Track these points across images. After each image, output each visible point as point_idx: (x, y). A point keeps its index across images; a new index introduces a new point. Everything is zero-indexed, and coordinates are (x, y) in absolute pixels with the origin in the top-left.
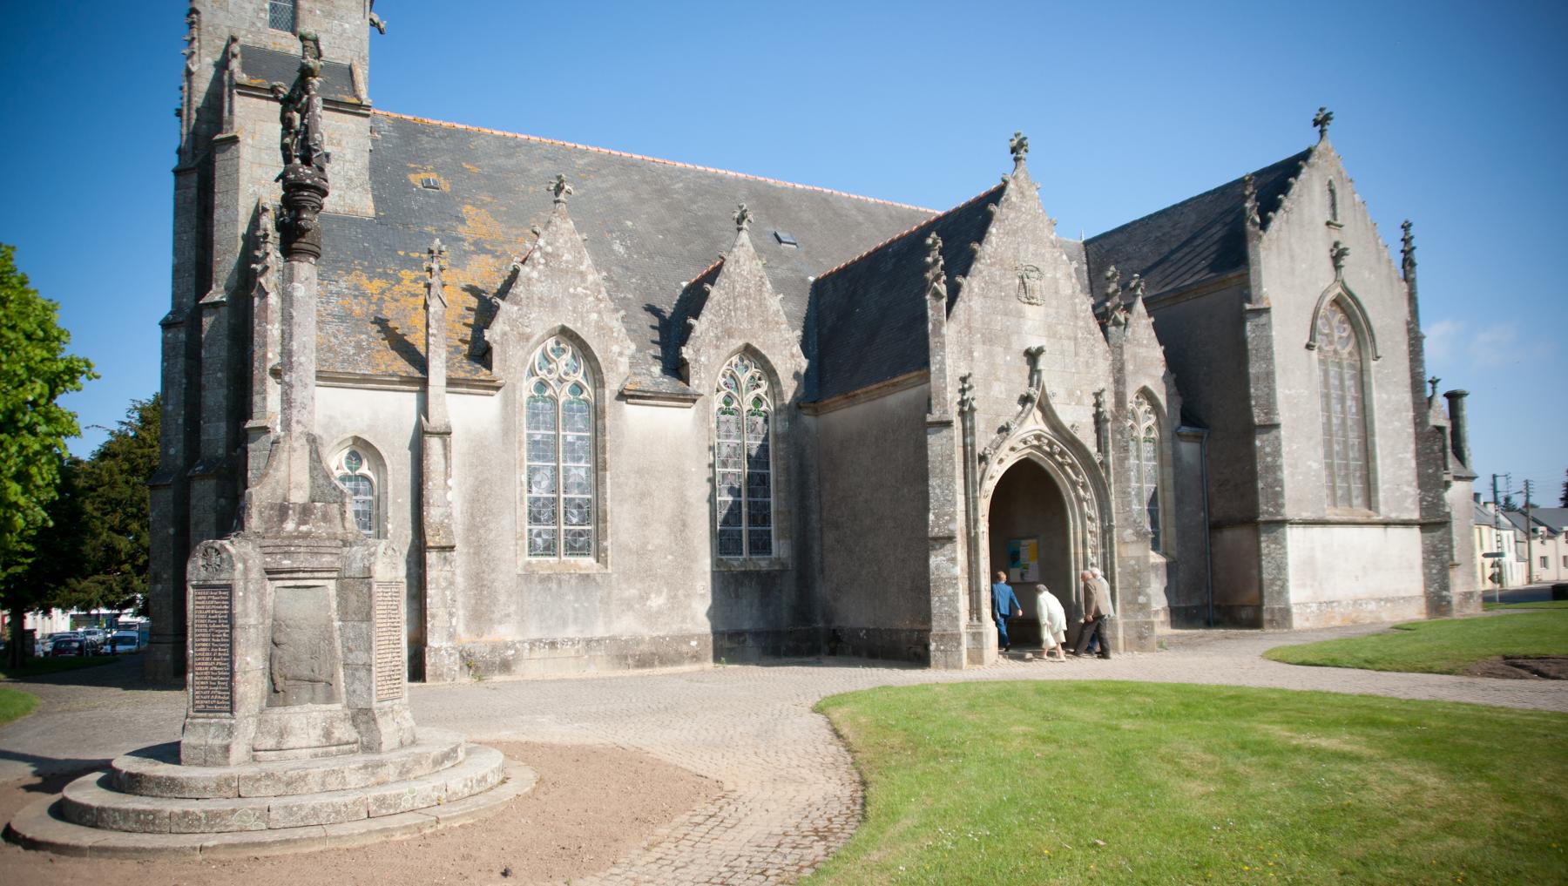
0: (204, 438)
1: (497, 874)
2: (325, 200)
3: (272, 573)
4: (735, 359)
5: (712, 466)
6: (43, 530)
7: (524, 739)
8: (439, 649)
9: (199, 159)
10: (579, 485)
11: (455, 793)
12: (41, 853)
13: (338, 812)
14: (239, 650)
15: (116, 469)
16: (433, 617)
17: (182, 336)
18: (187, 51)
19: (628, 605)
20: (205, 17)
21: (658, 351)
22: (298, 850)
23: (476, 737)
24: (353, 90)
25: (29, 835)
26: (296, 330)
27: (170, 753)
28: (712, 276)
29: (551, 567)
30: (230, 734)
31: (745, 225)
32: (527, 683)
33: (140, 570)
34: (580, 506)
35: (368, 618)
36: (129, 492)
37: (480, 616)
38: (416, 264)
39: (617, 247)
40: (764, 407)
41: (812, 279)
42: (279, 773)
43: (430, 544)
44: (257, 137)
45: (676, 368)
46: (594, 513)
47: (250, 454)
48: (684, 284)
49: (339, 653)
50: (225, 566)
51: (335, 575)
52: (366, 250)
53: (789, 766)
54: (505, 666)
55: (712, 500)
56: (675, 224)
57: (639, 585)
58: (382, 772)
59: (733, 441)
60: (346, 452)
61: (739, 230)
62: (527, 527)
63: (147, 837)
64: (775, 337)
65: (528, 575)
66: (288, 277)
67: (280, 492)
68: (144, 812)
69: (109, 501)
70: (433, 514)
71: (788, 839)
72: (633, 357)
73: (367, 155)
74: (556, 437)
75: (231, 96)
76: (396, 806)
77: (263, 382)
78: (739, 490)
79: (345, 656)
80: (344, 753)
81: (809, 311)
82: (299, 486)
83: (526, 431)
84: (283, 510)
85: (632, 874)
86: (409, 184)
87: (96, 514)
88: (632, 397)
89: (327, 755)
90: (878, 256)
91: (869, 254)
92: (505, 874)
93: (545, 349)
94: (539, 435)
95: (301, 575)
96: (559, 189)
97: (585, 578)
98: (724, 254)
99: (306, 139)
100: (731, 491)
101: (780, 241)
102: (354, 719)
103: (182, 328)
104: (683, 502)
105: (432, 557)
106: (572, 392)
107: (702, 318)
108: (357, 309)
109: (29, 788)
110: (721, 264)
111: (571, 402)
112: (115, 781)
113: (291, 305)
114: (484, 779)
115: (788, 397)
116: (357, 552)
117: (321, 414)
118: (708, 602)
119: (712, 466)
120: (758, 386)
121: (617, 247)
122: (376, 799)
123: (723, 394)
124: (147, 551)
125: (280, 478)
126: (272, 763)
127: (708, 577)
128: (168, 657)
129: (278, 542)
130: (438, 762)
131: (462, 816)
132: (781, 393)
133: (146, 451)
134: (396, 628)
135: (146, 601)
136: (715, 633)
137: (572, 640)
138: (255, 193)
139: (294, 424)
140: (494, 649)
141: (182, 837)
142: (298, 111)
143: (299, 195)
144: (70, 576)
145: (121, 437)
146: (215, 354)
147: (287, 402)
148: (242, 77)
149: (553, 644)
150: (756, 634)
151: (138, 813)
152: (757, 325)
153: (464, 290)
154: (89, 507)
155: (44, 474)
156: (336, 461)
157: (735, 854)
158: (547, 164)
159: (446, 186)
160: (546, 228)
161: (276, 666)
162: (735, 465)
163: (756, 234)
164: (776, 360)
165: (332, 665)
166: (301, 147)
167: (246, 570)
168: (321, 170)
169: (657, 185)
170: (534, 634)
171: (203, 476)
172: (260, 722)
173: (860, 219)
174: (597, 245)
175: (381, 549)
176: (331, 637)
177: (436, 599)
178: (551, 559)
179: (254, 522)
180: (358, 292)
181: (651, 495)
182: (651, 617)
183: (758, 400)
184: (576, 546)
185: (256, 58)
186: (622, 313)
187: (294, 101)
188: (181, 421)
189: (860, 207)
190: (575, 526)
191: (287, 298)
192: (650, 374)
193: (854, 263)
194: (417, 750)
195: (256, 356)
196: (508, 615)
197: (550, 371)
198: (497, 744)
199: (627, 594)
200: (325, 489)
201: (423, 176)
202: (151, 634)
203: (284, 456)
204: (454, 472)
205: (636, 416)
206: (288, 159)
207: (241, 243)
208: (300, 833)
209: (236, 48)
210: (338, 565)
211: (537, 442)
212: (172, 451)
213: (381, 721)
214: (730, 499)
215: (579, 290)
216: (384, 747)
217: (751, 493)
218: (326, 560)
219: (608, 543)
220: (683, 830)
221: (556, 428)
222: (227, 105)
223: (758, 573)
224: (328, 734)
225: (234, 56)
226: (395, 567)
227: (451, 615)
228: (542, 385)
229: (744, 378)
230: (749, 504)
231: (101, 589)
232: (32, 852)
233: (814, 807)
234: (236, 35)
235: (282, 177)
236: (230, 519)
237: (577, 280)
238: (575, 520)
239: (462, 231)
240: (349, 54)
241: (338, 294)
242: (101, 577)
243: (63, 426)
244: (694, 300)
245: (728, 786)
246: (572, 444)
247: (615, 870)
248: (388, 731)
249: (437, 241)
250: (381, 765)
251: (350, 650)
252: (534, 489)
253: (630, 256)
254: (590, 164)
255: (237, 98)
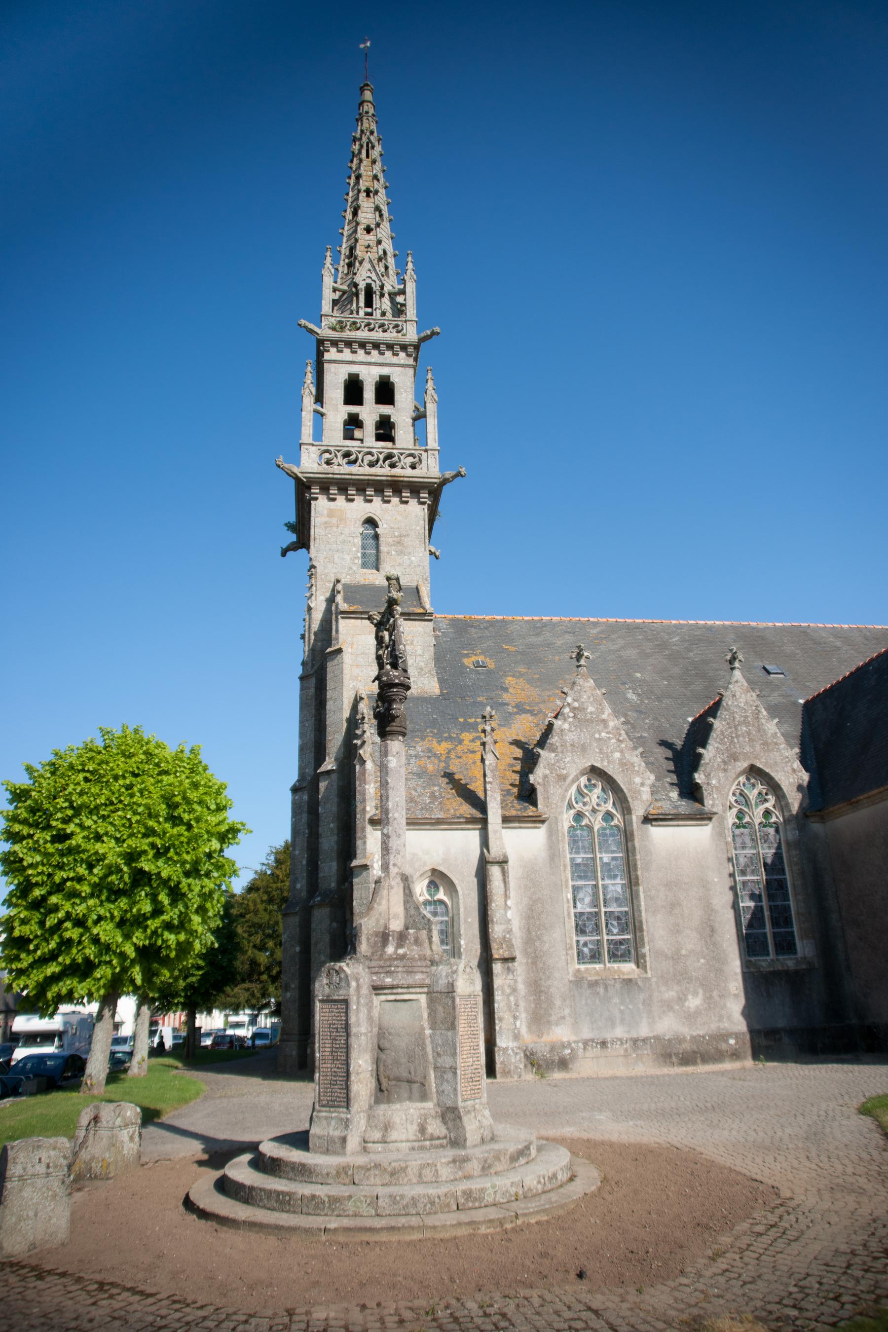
0: (321, 875)
1: (572, 1276)
2: (408, 693)
3: (377, 989)
4: (742, 779)
5: (732, 875)
6: (211, 950)
7: (585, 1136)
8: (506, 1049)
9: (316, 668)
10: (617, 899)
11: (530, 1189)
12: (209, 1223)
13: (433, 1203)
14: (354, 1054)
15: (258, 901)
16: (501, 1020)
17: (305, 797)
18: (308, 595)
19: (668, 1006)
20: (319, 570)
21: (673, 778)
22: (401, 1238)
23: (543, 1133)
24: (420, 604)
25: (201, 1206)
26: (391, 793)
27: (300, 1140)
28: (713, 710)
29: (597, 973)
30: (347, 1126)
31: (737, 664)
32: (584, 1080)
33: (274, 979)
34: (618, 918)
35: (453, 1026)
36: (267, 917)
37: (540, 1018)
38: (473, 727)
39: (631, 695)
40: (774, 819)
41: (802, 701)
42: (385, 1164)
43: (496, 956)
44: (355, 646)
45: (691, 792)
46: (631, 923)
47: (355, 887)
48: (690, 719)
49: (430, 1057)
50: (343, 984)
51: (426, 990)
52: (435, 720)
53: (844, 1173)
54: (563, 1064)
55: (735, 906)
56: (676, 671)
57: (676, 988)
58: (468, 1167)
59: (749, 852)
60: (426, 882)
61: (733, 669)
62: (575, 938)
63: (284, 1215)
64: (775, 756)
65: (579, 981)
66: (385, 753)
67: (382, 922)
68: (283, 1193)
69: (254, 925)
70: (496, 931)
71: (857, 1260)
72: (653, 786)
73: (432, 649)
74: (594, 859)
75: (337, 621)
76: (481, 1199)
77: (363, 829)
78: (760, 896)
79: (435, 1060)
80: (436, 1147)
81: (803, 729)
82: (396, 916)
83: (568, 856)
84: (384, 937)
85: (701, 1286)
86: (463, 666)
87: (246, 935)
88: (656, 820)
89: (422, 1148)
90: (859, 674)
91: (852, 674)
92: (581, 1275)
93: (579, 787)
94: (579, 858)
95: (400, 990)
96: (579, 656)
97: (628, 982)
98: (722, 691)
99: (394, 650)
100: (752, 896)
101: (769, 673)
102: (443, 1117)
103: (305, 789)
104: (709, 910)
105: (497, 967)
106: (604, 819)
107: (710, 747)
108: (430, 767)
109: (201, 1163)
110: (720, 701)
111: (604, 829)
112: (264, 1164)
113: (387, 774)
114: (555, 1176)
115: (795, 807)
116: (443, 970)
117: (409, 853)
118: (742, 1001)
119: (732, 875)
120: (766, 800)
121: (631, 695)
122: (464, 1192)
123: (735, 811)
124: (280, 963)
125: (381, 910)
126: (379, 1154)
127: (740, 977)
128: (294, 1053)
129: (382, 963)
130: (514, 1158)
131: (538, 1212)
132: (787, 805)
133: (279, 885)
134: (475, 1035)
135: (278, 1004)
136: (751, 1031)
137: (621, 1040)
138: (354, 687)
139: (391, 867)
140: (552, 1049)
141: (311, 1218)
142: (387, 630)
143: (389, 692)
144: (226, 985)
145: (263, 874)
146: (328, 810)
147: (386, 849)
148: (344, 606)
149: (604, 1044)
150: (791, 1032)
151: (278, 1193)
152: (758, 747)
153: (511, 744)
154: (240, 930)
155: (215, 908)
156: (420, 889)
157: (803, 1271)
158: (567, 637)
159: (491, 664)
160: (572, 688)
161: (381, 1068)
162: (753, 872)
163: (747, 670)
164: (779, 776)
165: (425, 1068)
166: (390, 655)
167: (358, 987)
168: (405, 671)
169: (657, 640)
170: (587, 1034)
171: (320, 905)
172: (369, 1118)
173: (838, 644)
174: (614, 696)
175: (461, 967)
176: (424, 1043)
177: (502, 1005)
178: (598, 966)
179: (364, 947)
180: (431, 754)
181: (680, 905)
182: (691, 1017)
183: (767, 813)
184: (618, 953)
185: (354, 592)
186: (641, 750)
187: (384, 624)
188: (304, 862)
189: (837, 633)
190: (615, 935)
191: (383, 768)
192: (669, 799)
193: (838, 683)
194: (496, 1146)
195: (358, 810)
196: (563, 1018)
197: (585, 804)
198: (561, 1141)
199: (667, 995)
200: (415, 918)
201: (474, 659)
202: (283, 1032)
203: (385, 892)
204: (512, 893)
205: (659, 834)
206: (381, 666)
207: (345, 725)
208: (402, 1221)
209: (339, 587)
210: (427, 981)
211: (578, 865)
212: (298, 886)
213: (465, 1119)
214: (752, 904)
215: (603, 734)
216: (468, 1143)
217: (771, 897)
218: (419, 977)
219: (646, 950)
220: (746, 1240)
221: (593, 851)
222: (334, 627)
223: (787, 972)
224: (422, 1129)
225: (339, 592)
226: (472, 983)
227: (515, 1018)
228: (579, 816)
229: (753, 794)
230: (771, 909)
231: (246, 994)
232: (203, 1221)
233: (879, 1224)
234: (339, 578)
235: (378, 678)
236: (344, 943)
237: (601, 727)
238: (615, 931)
239: (506, 697)
240: (416, 578)
241: (416, 756)
242: (247, 985)
243: (226, 869)
244: (700, 732)
245: (786, 1193)
246: (608, 864)
247: (684, 1281)
248: (472, 1128)
249: (488, 708)
250: (466, 1159)
251: (439, 1055)
252: (579, 905)
253: (642, 701)
254: (602, 632)
255: (341, 621)
